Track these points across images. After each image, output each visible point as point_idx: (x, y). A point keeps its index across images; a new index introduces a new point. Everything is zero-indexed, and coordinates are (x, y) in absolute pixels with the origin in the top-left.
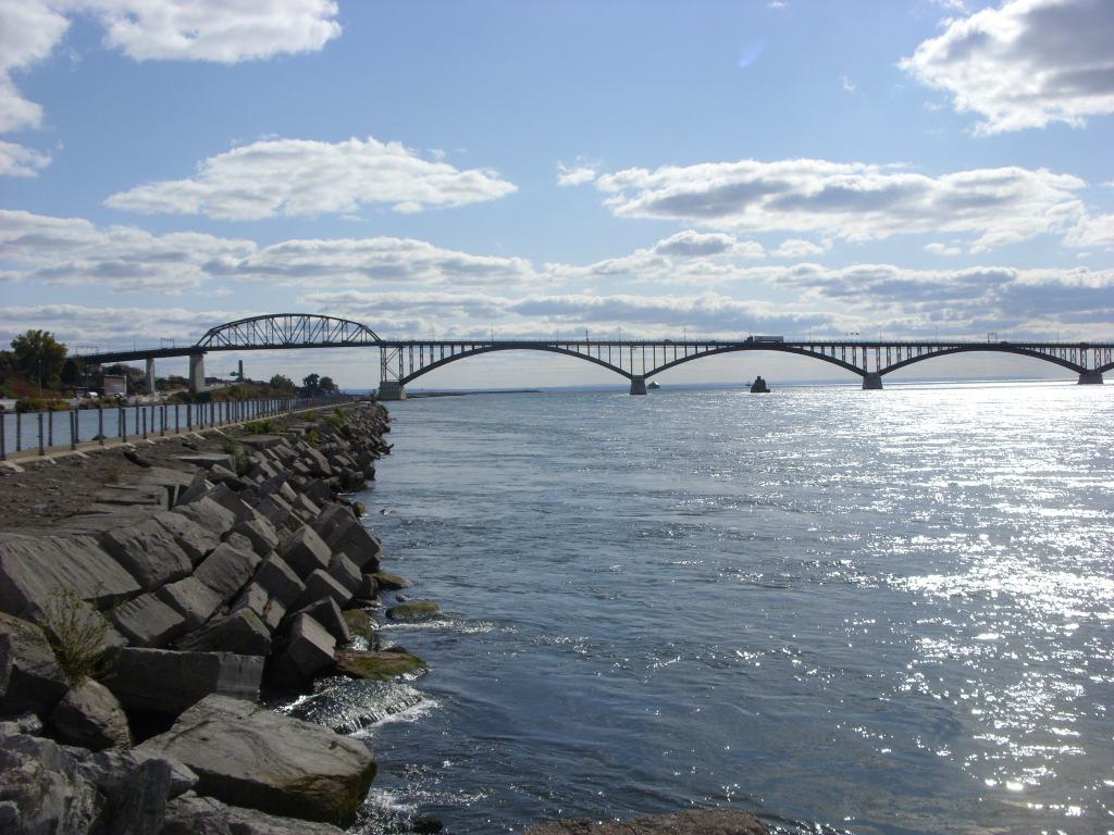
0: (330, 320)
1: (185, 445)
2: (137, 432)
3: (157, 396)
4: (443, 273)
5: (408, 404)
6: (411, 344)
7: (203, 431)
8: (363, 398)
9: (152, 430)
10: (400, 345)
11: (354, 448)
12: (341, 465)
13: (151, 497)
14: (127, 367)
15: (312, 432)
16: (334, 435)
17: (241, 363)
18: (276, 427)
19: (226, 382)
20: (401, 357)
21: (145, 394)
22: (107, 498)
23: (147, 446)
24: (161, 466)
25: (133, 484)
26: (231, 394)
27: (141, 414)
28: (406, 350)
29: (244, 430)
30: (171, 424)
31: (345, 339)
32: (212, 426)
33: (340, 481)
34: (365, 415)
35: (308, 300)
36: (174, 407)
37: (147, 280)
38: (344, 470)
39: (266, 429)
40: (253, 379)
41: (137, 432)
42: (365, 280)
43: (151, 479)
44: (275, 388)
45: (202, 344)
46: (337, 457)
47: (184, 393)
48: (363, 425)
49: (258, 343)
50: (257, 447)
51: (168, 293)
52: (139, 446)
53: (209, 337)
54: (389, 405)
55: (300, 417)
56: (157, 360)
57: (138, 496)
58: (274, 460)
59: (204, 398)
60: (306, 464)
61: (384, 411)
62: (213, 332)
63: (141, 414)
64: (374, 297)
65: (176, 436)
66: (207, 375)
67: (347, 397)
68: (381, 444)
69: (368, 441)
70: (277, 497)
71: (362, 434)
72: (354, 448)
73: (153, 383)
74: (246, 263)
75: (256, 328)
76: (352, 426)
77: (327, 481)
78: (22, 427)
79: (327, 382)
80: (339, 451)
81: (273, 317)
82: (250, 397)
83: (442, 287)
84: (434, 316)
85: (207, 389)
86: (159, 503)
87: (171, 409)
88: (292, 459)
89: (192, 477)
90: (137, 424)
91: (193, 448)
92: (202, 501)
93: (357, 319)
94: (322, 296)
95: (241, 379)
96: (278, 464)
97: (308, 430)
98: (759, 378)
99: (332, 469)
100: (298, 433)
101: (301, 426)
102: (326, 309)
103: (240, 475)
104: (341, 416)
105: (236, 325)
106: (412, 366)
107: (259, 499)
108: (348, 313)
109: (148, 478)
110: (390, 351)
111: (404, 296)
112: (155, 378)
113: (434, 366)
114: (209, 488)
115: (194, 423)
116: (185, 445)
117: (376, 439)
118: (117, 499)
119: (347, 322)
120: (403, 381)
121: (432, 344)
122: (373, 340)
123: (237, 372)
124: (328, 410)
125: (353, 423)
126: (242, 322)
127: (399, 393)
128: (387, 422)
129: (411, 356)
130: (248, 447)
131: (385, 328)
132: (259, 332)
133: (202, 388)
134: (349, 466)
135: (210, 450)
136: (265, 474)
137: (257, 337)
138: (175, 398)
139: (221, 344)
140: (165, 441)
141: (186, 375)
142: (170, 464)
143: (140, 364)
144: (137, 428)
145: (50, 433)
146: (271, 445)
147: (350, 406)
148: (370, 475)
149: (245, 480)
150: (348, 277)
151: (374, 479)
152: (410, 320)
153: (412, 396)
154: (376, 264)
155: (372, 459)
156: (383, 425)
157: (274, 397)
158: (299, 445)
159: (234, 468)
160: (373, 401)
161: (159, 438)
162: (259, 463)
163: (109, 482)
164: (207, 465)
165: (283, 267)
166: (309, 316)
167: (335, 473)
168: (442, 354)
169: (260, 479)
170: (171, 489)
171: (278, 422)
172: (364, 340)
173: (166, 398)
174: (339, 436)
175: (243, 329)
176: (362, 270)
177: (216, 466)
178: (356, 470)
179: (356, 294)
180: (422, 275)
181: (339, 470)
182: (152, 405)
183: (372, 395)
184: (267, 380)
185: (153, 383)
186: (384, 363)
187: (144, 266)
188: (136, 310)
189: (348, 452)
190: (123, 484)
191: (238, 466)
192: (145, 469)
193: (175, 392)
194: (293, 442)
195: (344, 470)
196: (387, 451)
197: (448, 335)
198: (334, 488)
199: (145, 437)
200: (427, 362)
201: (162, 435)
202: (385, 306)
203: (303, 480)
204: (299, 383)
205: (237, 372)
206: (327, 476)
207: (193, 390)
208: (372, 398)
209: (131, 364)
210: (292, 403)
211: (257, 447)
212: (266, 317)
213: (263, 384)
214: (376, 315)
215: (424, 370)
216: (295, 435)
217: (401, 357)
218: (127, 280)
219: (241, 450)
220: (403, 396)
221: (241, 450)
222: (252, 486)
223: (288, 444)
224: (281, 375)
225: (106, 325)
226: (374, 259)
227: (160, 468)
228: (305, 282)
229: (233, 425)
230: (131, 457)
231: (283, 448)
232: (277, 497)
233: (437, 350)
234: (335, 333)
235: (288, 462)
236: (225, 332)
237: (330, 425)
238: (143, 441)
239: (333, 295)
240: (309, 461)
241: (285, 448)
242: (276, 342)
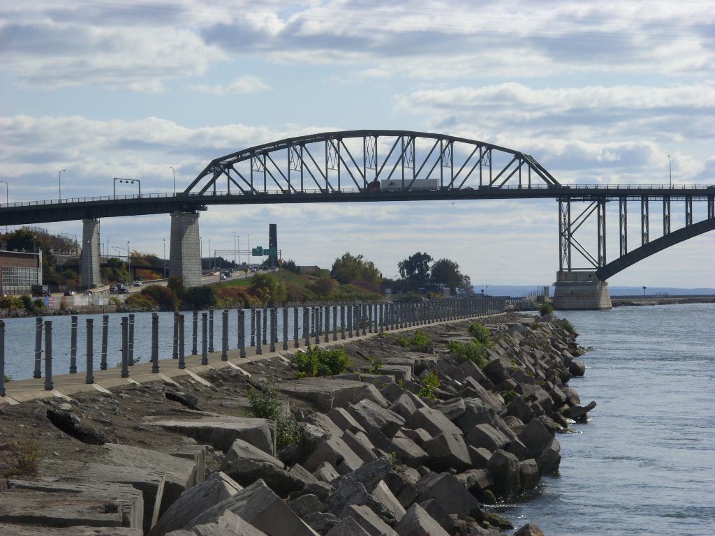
0: (456, 144)
1: (171, 397)
2: (73, 369)
3: (101, 295)
4: (706, 46)
5: (617, 317)
6: (623, 194)
7: (209, 367)
8: (522, 305)
9: (104, 366)
10: (599, 196)
11: (513, 409)
12: (489, 444)
13: (111, 508)
14: (44, 236)
15: (426, 373)
16: (470, 379)
17: (273, 229)
18: (351, 361)
19: (244, 267)
20: (602, 220)
21: (83, 289)
22: (17, 512)
23: (95, 397)
24: (124, 440)
25: (67, 480)
26: (252, 292)
27: (200, 324)
28: (612, 207)
29: (291, 368)
30: (142, 351)
31: (486, 182)
32: (225, 358)
33: (488, 477)
34: (528, 341)
35: (416, 104)
36: (148, 316)
37: (100, 60)
38: (497, 456)
39: (332, 366)
40: (297, 264)
41: (73, 369)
42: (539, 61)
43: (107, 470)
44: (343, 281)
45: (196, 190)
46: (480, 427)
47: (159, 289)
48: (528, 360)
49: (311, 188)
50: (316, 402)
51: (136, 86)
52: (78, 399)
53: (210, 176)
54: (577, 320)
55: (398, 342)
56: (104, 222)
57: (84, 507)
58: (355, 430)
59: (200, 300)
60: (418, 441)
61: (567, 331)
62: (219, 166)
63: (200, 324)
64: (559, 98)
65: (154, 377)
66: (206, 253)
67: (487, 302)
68: (568, 401)
69: (542, 395)
70: (365, 511)
71: (526, 380)
72: (513, 409)
73: (96, 267)
74: (298, 25)
75: (307, 160)
76: (506, 364)
77: (462, 477)
78: (109, 335)
79: (447, 271)
80: (486, 416)
81: (340, 136)
82: (290, 299)
83: (701, 74)
84: (678, 137)
85: (206, 281)
86: (126, 523)
87: (143, 320)
88: (390, 429)
89: (190, 466)
90: (74, 352)
91: (189, 403)
92: (220, 519)
93: (520, 143)
94: (446, 95)
95: (273, 261)
96: (362, 438)
97: (418, 369)
99: (473, 454)
100: (399, 375)
101: (405, 362)
102: (451, 122)
103: (289, 463)
104: (482, 341)
105: (265, 153)
106: (623, 240)
107: (331, 517)
108: (497, 130)
109: (97, 468)
110: (578, 207)
111: (620, 95)
112: (104, 253)
113: (671, 239)
114: (233, 492)
115: (247, 343)
116: (171, 397)
117: (558, 390)
118: (37, 513)
119: (490, 147)
120: (606, 271)
121: (667, 195)
122: (544, 185)
123: (266, 246)
124: (454, 328)
125: (510, 355)
126: (277, 146)
127: (595, 296)
128: (576, 355)
129: (623, 219)
130: (297, 401)
131: (573, 160)
132: (312, 167)
133: (194, 278)
134: (507, 447)
135: (223, 409)
136: (338, 462)
137: (307, 178)
138: (142, 299)
139: (235, 191)
140: (132, 389)
141: (162, 251)
142: (143, 438)
143: (72, 229)
144: (73, 360)
145: (104, 350)
146: (347, 398)
147: (496, 321)
148: (550, 466)
149: (297, 473)
150: (508, 56)
151: (557, 476)
152: (629, 144)
153: (622, 301)
154: (565, 29)
155: (553, 431)
156: (567, 362)
157: (339, 299)
158: (404, 400)
159: (273, 447)
160: (544, 312)
161: (120, 382)
162: (325, 437)
163: (19, 475)
164: (221, 440)
165: (380, 37)
166: (413, 135)
167: (478, 462)
168: (689, 216)
169: (329, 471)
170: (148, 490)
171: (358, 352)
172: (525, 184)
173: (122, 298)
174: (481, 382)
175: (279, 160)
176: (538, 41)
177: (239, 443)
178: (523, 455)
179: (527, 94)
180: (663, 51)
181: (486, 454)
182: (91, 310)
183: (540, 299)
184: (327, 264)
185: (96, 267)
186: (566, 233)
187: (98, 32)
188: (78, 120)
189: (503, 417)
190: (48, 481)
191: (281, 444)
192: (95, 447)
193: (142, 286)
194: (391, 394)
195: (497, 456)
196: (581, 416)
197: (704, 175)
198: (475, 490)
199: (90, 380)
200: (656, 232)
201: (125, 375)
202: (581, 116)
203: (412, 476)
204: (390, 271)
205: (267, 248)
206: (462, 468)
207: (176, 283)
208: (543, 304)
209: (54, 228)
210: (375, 313)
211: (316, 402)
212: (326, 137)
213: (316, 271)
214: (557, 135)
215: (649, 249)
216: (393, 377)
217: (602, 220)
218: (51, 60)
219: (285, 409)
220: (605, 302)
221: (285, 409)
222: (315, 488)
223: (384, 401)
224: (354, 254)
225: (10, 150)
226: (561, 17)
227: (125, 447)
228: (418, 66)
229: (267, 356)
230: (62, 422)
231: (372, 406)
232: (365, 511)
233: (678, 206)
234: (466, 171)
235: (383, 434)
236: (243, 167)
237: (460, 361)
238: (88, 388)
239: (469, 93)
240: (425, 435)
241: (374, 407)
242: (348, 187)
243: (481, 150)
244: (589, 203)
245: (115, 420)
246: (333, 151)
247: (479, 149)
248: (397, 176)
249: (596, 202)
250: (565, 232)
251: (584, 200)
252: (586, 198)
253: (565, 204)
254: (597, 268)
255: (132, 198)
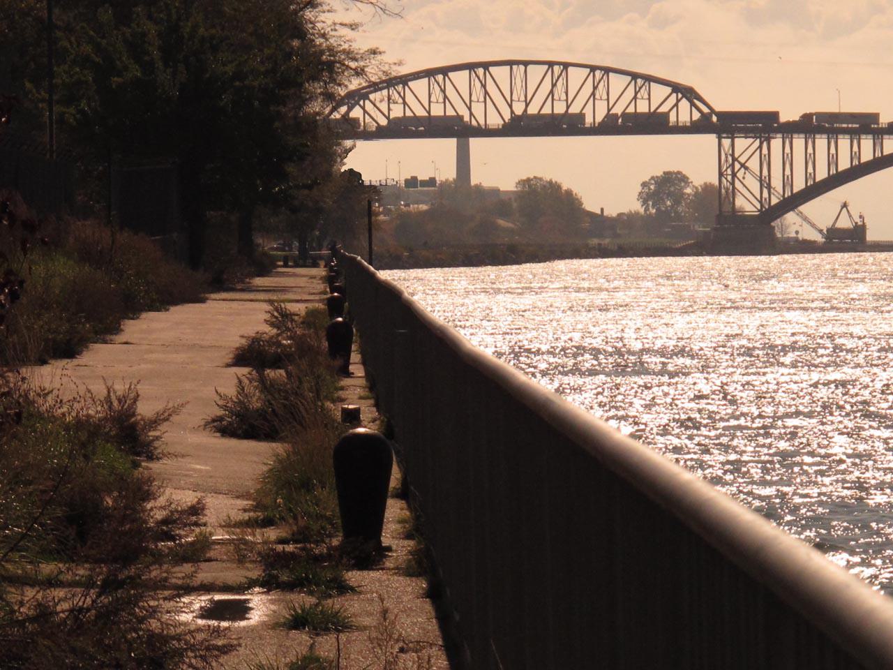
98: (123, 331)
243: (594, 76)
244: (750, 140)
245: (532, 285)
246: (478, 85)
247: (633, 82)
248: (547, 110)
249: (758, 140)
250: (726, 170)
251: (746, 137)
252: (748, 135)
253: (726, 142)
254: (759, 211)
255: (497, 127)
